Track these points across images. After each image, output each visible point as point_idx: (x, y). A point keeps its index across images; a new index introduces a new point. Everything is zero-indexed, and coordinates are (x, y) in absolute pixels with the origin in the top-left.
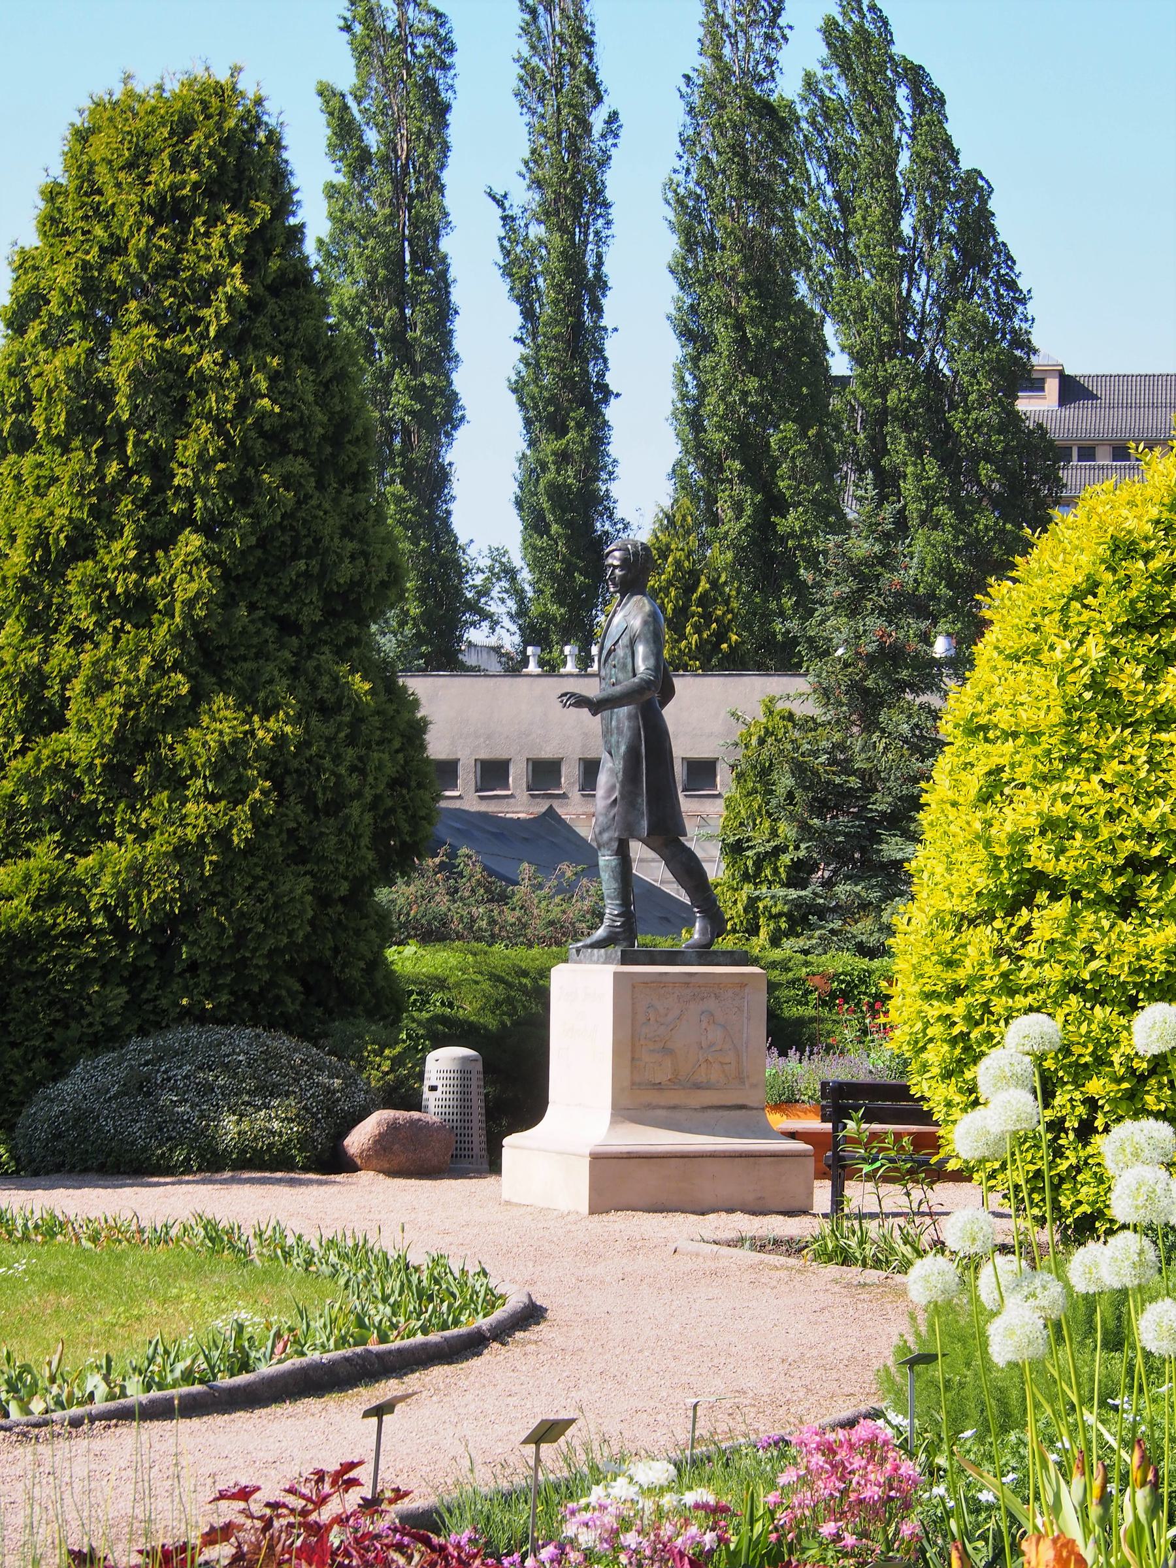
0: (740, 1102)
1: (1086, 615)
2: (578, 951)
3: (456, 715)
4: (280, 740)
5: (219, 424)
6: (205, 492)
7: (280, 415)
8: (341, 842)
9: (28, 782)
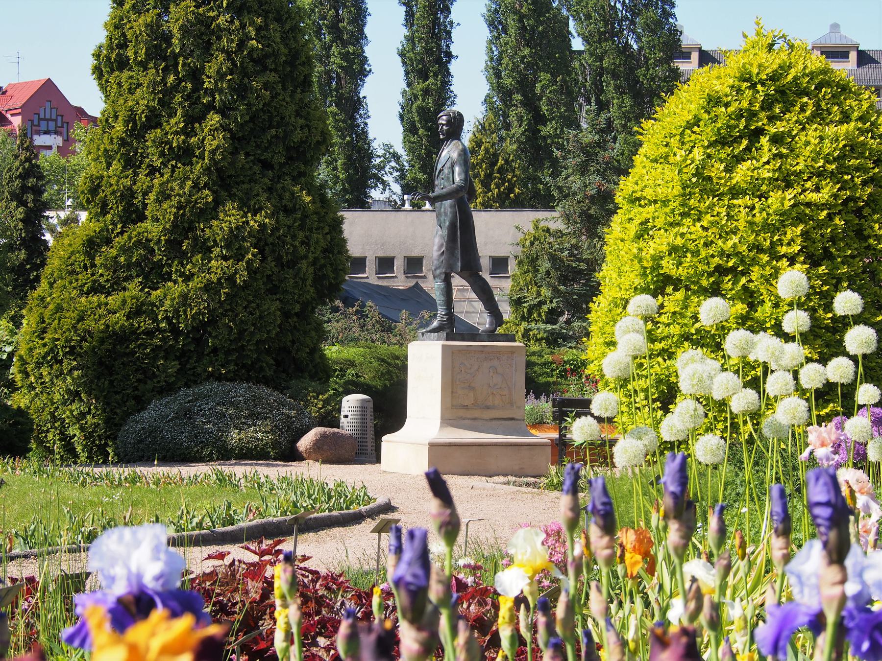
0: (511, 416)
1: (693, 137)
2: (423, 334)
3: (363, 232)
4: (263, 226)
5: (228, 54)
6: (221, 91)
7: (262, 49)
8: (296, 282)
9: (124, 250)
